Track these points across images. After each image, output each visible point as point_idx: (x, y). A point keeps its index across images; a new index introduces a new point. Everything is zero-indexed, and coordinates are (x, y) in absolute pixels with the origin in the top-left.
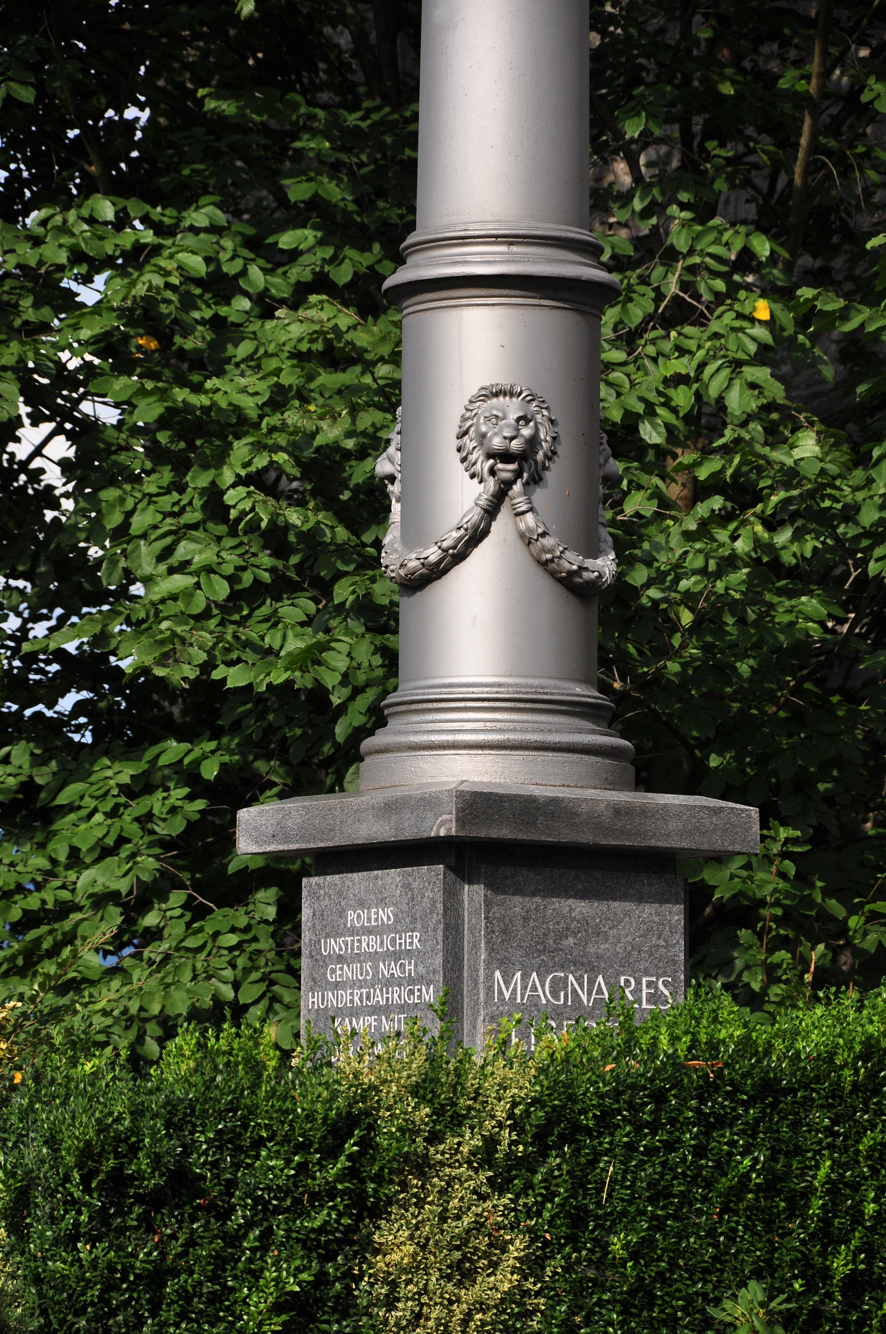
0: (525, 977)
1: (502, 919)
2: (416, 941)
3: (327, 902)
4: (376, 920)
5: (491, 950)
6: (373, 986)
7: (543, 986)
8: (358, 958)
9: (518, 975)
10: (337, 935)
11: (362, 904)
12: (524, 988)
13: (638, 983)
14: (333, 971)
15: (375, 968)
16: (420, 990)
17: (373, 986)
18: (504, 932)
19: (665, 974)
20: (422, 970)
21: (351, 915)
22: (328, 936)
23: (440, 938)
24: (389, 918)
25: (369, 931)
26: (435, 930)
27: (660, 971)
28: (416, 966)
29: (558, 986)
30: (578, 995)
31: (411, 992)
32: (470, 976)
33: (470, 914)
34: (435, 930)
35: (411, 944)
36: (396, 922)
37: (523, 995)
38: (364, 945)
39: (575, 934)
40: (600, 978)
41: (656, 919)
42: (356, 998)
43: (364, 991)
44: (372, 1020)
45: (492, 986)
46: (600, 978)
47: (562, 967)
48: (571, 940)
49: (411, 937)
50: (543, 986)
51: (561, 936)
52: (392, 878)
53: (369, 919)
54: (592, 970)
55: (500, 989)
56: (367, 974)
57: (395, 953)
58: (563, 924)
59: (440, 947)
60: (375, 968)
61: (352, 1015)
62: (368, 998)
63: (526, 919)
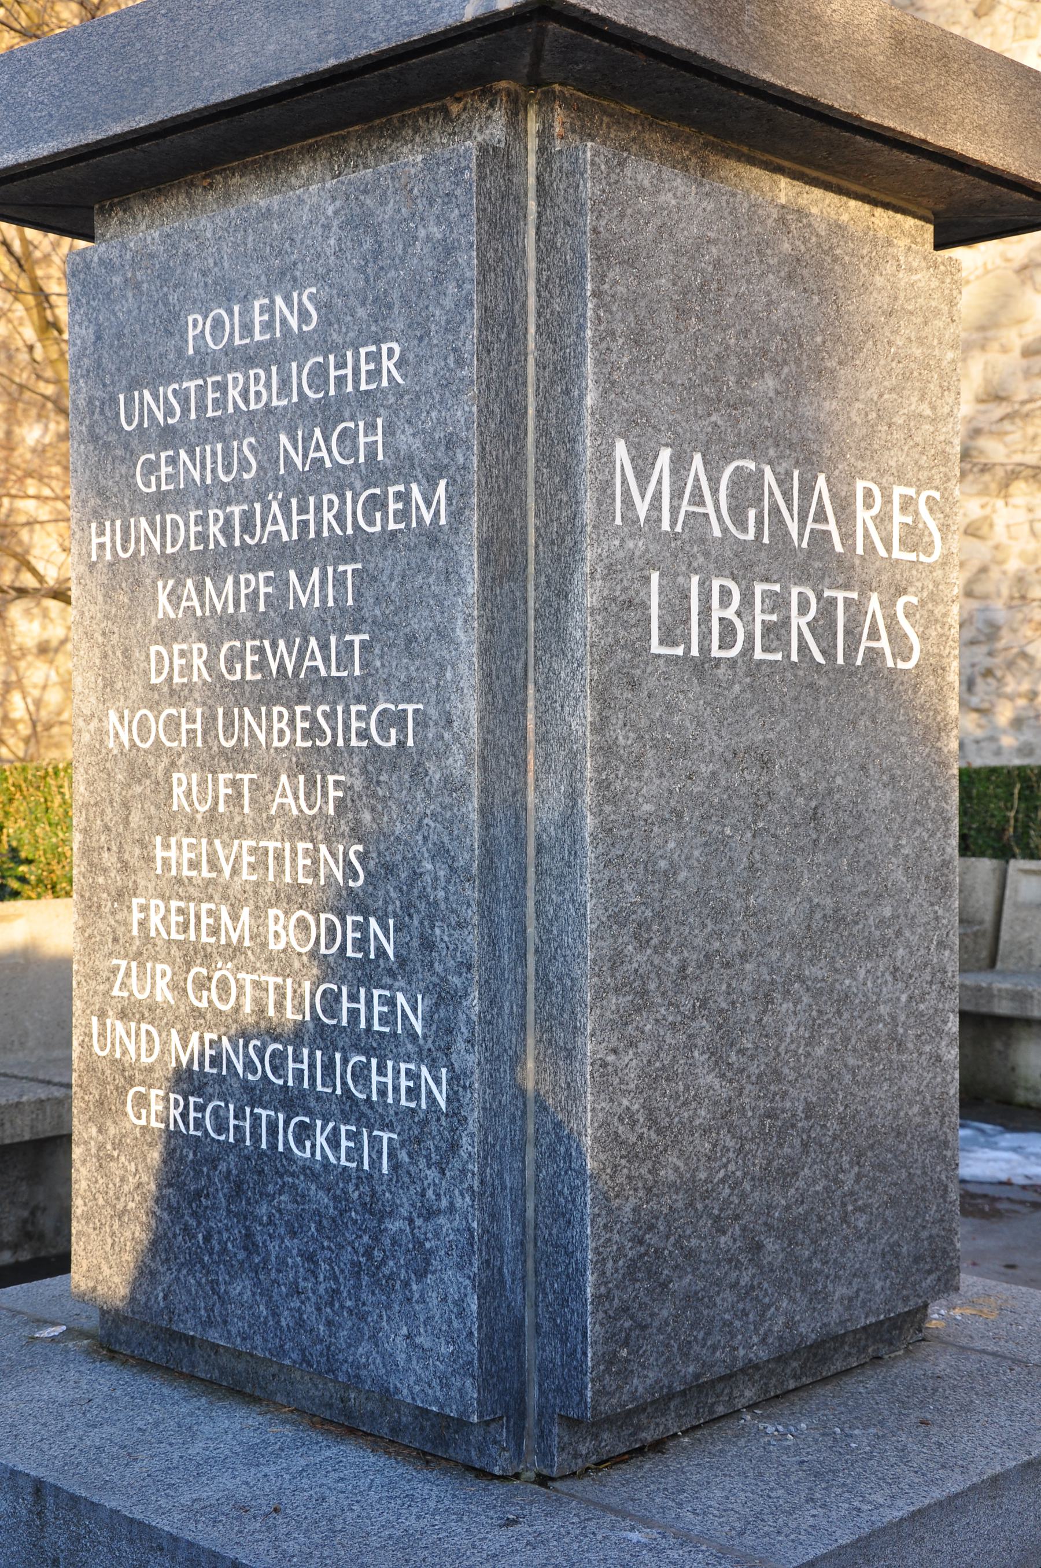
0: (680, 464)
1: (631, 302)
2: (387, 364)
3: (130, 301)
4: (268, 326)
5: (608, 386)
6: (261, 496)
7: (715, 492)
8: (217, 430)
9: (665, 456)
10: (158, 377)
11: (228, 292)
12: (677, 494)
13: (887, 500)
14: (151, 467)
15: (267, 450)
16: (404, 497)
17: (261, 496)
18: (637, 340)
19: (929, 483)
20: (407, 440)
21: (196, 326)
22: (135, 384)
23: (470, 347)
24: (304, 316)
25: (247, 358)
26: (451, 328)
27: (923, 475)
28: (390, 431)
29: (745, 493)
30: (782, 521)
31: (377, 503)
32: (545, 456)
33: (542, 286)
34: (451, 328)
35: (374, 375)
36: (325, 321)
37: (674, 511)
38: (233, 393)
39: (778, 365)
40: (822, 479)
41: (917, 352)
42: (214, 529)
43: (236, 510)
44: (260, 582)
45: (609, 483)
46: (822, 479)
47: (752, 447)
48: (770, 383)
49: (375, 357)
50: (715, 492)
51: (750, 370)
52: (308, 197)
53: (247, 329)
54: (808, 460)
55: (626, 492)
56: (245, 466)
57: (324, 404)
58: (754, 339)
59: (470, 372)
60: (267, 450)
61: (202, 571)
62: (248, 527)
63: (682, 312)
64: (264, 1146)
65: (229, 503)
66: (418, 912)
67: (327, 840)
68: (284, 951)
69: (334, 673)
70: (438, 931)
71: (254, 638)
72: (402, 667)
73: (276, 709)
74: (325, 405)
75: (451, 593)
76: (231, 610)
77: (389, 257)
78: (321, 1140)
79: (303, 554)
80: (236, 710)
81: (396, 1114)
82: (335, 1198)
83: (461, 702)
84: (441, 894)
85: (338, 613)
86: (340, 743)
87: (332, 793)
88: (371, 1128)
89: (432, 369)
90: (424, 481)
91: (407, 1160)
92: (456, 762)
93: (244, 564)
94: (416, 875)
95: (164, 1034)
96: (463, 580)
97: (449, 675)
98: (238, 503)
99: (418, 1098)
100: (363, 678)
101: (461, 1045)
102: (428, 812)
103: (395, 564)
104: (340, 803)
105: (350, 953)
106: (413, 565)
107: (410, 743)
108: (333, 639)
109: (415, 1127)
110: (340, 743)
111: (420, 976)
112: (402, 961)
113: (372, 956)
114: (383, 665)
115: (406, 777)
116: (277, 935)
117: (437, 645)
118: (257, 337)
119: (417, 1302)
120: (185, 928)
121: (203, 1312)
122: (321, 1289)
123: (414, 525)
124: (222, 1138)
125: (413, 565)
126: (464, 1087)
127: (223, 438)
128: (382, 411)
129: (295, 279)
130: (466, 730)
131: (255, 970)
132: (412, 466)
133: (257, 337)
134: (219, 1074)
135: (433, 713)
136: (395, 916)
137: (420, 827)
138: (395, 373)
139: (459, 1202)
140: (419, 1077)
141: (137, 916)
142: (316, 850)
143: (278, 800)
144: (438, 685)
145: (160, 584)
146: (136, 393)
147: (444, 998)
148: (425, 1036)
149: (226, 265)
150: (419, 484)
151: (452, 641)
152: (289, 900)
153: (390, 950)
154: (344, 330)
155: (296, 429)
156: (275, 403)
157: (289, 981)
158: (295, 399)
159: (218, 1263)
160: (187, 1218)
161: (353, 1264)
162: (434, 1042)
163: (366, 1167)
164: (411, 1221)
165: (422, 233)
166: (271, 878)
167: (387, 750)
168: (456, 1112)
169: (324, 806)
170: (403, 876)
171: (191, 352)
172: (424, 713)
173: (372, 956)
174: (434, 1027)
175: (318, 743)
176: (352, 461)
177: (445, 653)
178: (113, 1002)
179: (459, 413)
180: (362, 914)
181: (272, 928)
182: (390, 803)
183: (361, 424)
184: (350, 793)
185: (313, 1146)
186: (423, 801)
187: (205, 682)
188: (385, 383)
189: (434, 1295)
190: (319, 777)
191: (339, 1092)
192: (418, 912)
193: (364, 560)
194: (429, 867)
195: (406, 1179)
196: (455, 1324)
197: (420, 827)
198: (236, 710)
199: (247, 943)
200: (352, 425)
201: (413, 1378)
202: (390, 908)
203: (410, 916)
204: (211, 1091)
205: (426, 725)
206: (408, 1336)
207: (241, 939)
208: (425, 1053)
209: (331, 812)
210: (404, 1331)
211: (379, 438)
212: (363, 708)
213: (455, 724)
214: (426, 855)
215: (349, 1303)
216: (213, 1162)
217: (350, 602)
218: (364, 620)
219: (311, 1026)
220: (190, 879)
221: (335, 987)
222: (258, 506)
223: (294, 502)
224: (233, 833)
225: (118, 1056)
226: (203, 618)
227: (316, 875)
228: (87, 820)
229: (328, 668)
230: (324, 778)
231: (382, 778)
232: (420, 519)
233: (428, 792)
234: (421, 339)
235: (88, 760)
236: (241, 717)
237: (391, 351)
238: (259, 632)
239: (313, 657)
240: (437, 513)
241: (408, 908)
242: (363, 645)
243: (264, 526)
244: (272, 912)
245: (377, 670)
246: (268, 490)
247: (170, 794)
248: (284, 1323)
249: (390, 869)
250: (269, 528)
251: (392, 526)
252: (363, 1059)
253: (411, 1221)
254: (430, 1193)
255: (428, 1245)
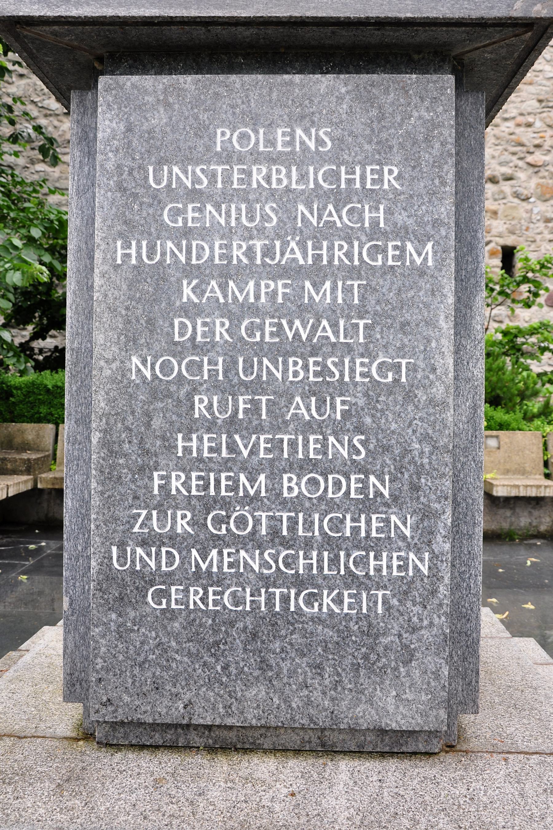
28: (389, 212)
34: (438, 164)
64: (277, 609)
65: (251, 238)
66: (408, 471)
67: (335, 433)
68: (297, 497)
69: (342, 340)
70: (423, 481)
71: (273, 317)
72: (397, 339)
73: (291, 360)
74: (337, 192)
75: (436, 302)
76: (252, 300)
77: (390, 122)
78: (326, 600)
79: (318, 273)
80: (255, 359)
81: (389, 580)
82: (338, 631)
83: (443, 359)
84: (425, 461)
85: (346, 307)
86: (347, 379)
87: (339, 407)
88: (368, 589)
89: (422, 184)
90: (416, 241)
91: (397, 604)
92: (438, 391)
93: (264, 274)
94: (407, 451)
95: (184, 553)
96: (445, 296)
97: (434, 345)
98: (259, 239)
99: (407, 570)
100: (366, 344)
101: (439, 539)
102: (417, 417)
103: (393, 283)
104: (344, 414)
105: (353, 495)
106: (407, 285)
107: (404, 379)
108: (342, 323)
109: (404, 589)
110: (347, 379)
111: (409, 505)
112: (395, 498)
113: (371, 496)
114: (382, 337)
115: (400, 398)
116: (290, 489)
117: (424, 328)
118: (280, 148)
119: (404, 677)
120: (206, 487)
121: (221, 710)
122: (327, 682)
123: (408, 263)
124: (240, 608)
125: (407, 285)
126: (442, 561)
127: (247, 200)
128: (383, 201)
129: (313, 122)
130: (446, 375)
131: (269, 509)
132: (407, 233)
133: (280, 148)
134: (237, 572)
135: (422, 364)
136: (390, 473)
137: (410, 425)
138: (393, 182)
139: (436, 620)
140: (407, 559)
141: (157, 482)
142: (325, 439)
143: (292, 411)
144: (425, 350)
145: (185, 282)
146: (166, 168)
147: (426, 514)
148: (412, 537)
149: (253, 105)
150: (412, 242)
151: (436, 327)
152: (301, 468)
153: (386, 493)
154: (353, 154)
155: (312, 202)
156: (294, 186)
157: (301, 515)
158: (312, 186)
159: (235, 681)
160: (206, 658)
161: (353, 664)
162: (419, 539)
163: (364, 611)
164: (400, 636)
165: (416, 114)
166: (286, 456)
167: (385, 384)
168: (435, 575)
169: (333, 415)
170: (397, 452)
171: (219, 149)
172: (415, 365)
173: (371, 496)
174: (420, 531)
175: (328, 379)
176: (359, 225)
177: (431, 333)
178: (133, 536)
179: (443, 209)
180: (363, 473)
181: (286, 484)
182: (387, 413)
183: (367, 207)
184: (354, 407)
185: (321, 605)
186: (412, 411)
187: (226, 342)
188: (386, 186)
189: (417, 671)
190: (328, 399)
191: (342, 572)
192: (408, 471)
193: (367, 279)
194: (417, 446)
195: (397, 614)
196: (433, 684)
197: (410, 425)
198: (255, 359)
199: (263, 494)
200: (359, 206)
201: (401, 717)
202: (386, 470)
203: (402, 473)
204: (229, 582)
205: (416, 371)
206: (397, 695)
207: (258, 492)
208: (412, 546)
209: (339, 417)
210: (394, 693)
211: (382, 215)
212: (366, 360)
213: (438, 371)
214: (415, 440)
215: (349, 686)
216: (232, 624)
217: (356, 301)
218: (367, 312)
219: (319, 539)
220: (210, 459)
221: (341, 516)
222: (278, 244)
223: (310, 244)
224: (251, 431)
225: (138, 568)
226: (226, 304)
227: (325, 453)
228: (107, 423)
229: (338, 337)
230: (332, 398)
231: (380, 399)
232: (412, 262)
233: (417, 407)
234: (414, 168)
235: (109, 386)
236: (260, 363)
237: (390, 172)
238: (277, 314)
239: (292, 251)
240: (426, 259)
241: (400, 469)
242: (366, 326)
243: (282, 254)
244: (285, 477)
245: (378, 340)
246: (287, 234)
247: (192, 407)
248: (294, 705)
249: (387, 449)
250: (287, 255)
251: (390, 262)
252: (364, 553)
253: (400, 636)
254: (415, 619)
255: (412, 646)
